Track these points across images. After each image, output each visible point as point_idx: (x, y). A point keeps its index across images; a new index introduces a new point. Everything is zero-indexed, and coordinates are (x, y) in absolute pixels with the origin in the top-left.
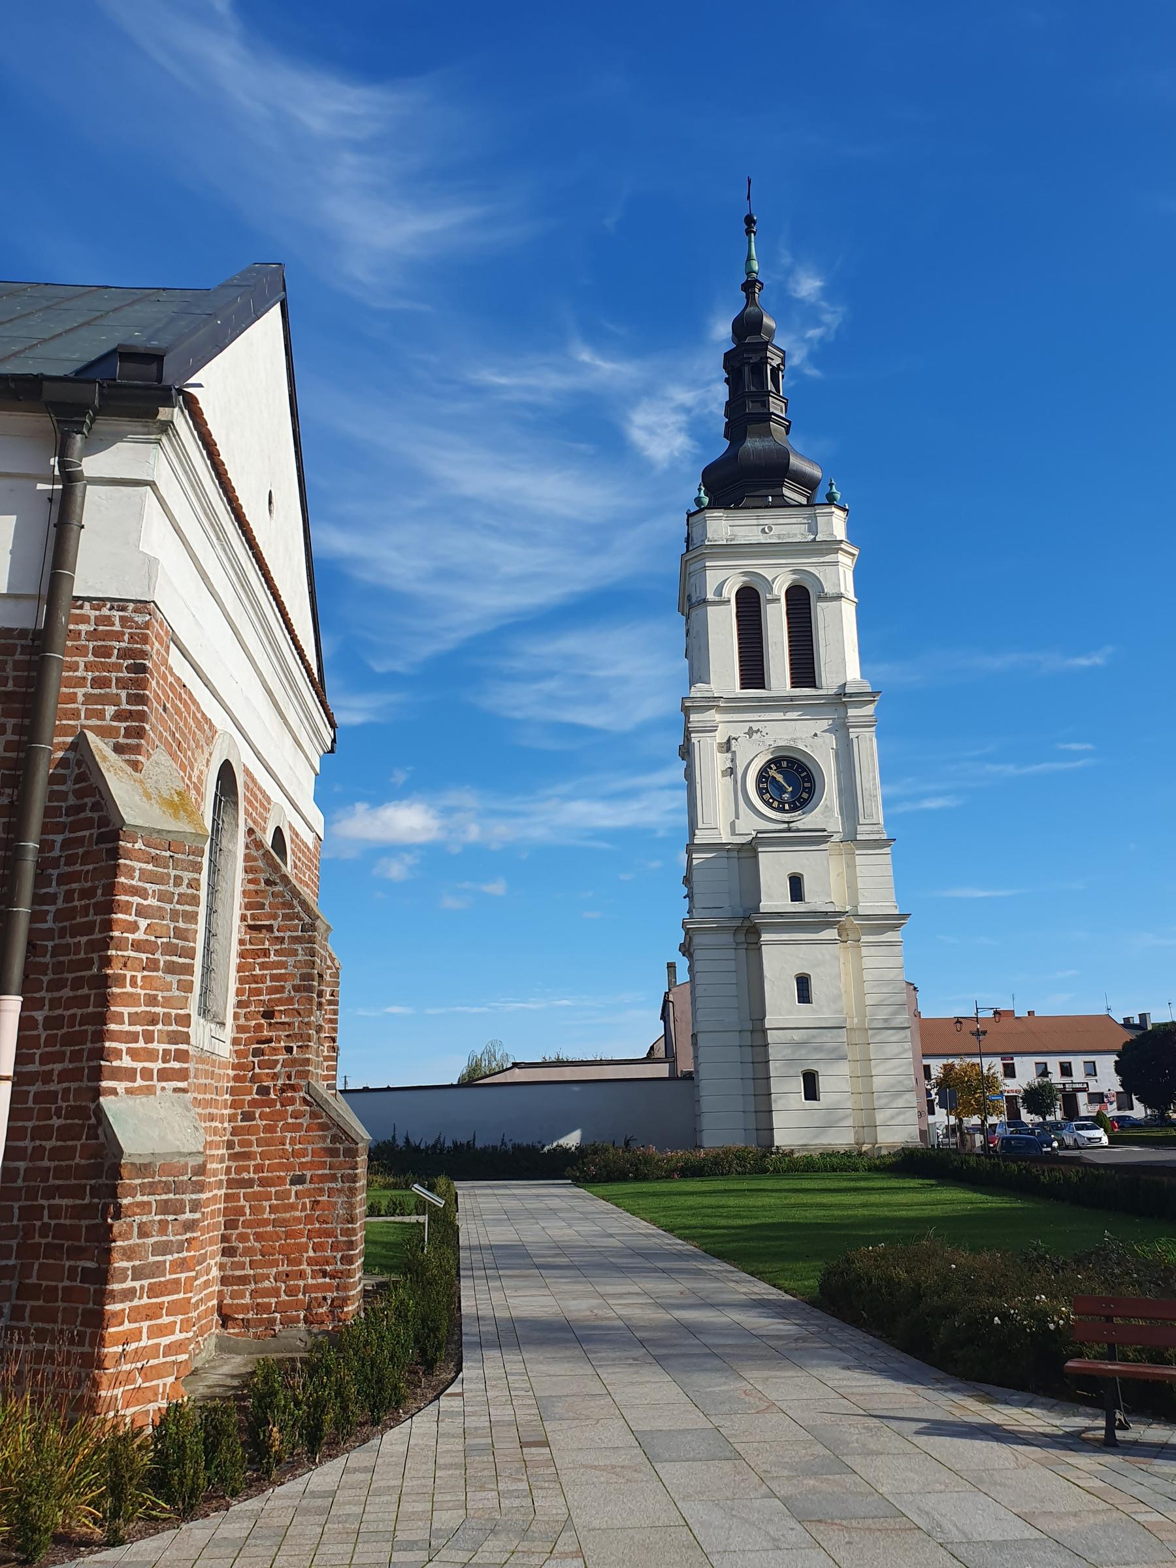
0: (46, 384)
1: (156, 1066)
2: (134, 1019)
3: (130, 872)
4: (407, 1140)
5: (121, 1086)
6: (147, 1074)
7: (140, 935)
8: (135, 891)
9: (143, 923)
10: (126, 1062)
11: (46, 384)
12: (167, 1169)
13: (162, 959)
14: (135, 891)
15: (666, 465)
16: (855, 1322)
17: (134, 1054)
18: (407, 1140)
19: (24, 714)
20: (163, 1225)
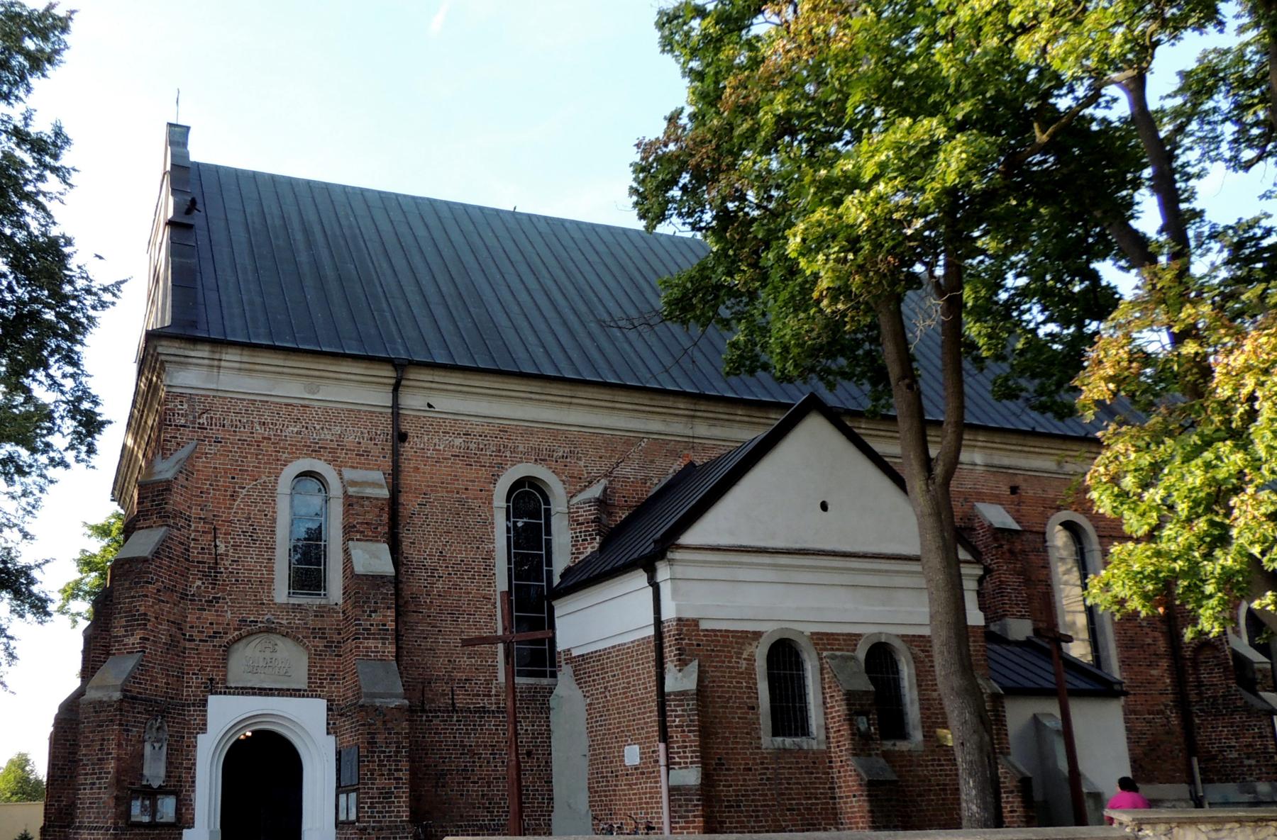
0: (303, 685)
1: (689, 760)
2: (678, 748)
3: (670, 706)
4: (103, 531)
5: (676, 767)
6: (686, 763)
7: (677, 723)
8: (672, 711)
9: (677, 720)
10: (677, 760)
11: (303, 685)
12: (685, 789)
13: (686, 729)
14: (672, 711)
15: (1268, 113)
16: (930, 827)
17: (679, 757)
18: (103, 531)
19: (703, 686)
20: (687, 805)
